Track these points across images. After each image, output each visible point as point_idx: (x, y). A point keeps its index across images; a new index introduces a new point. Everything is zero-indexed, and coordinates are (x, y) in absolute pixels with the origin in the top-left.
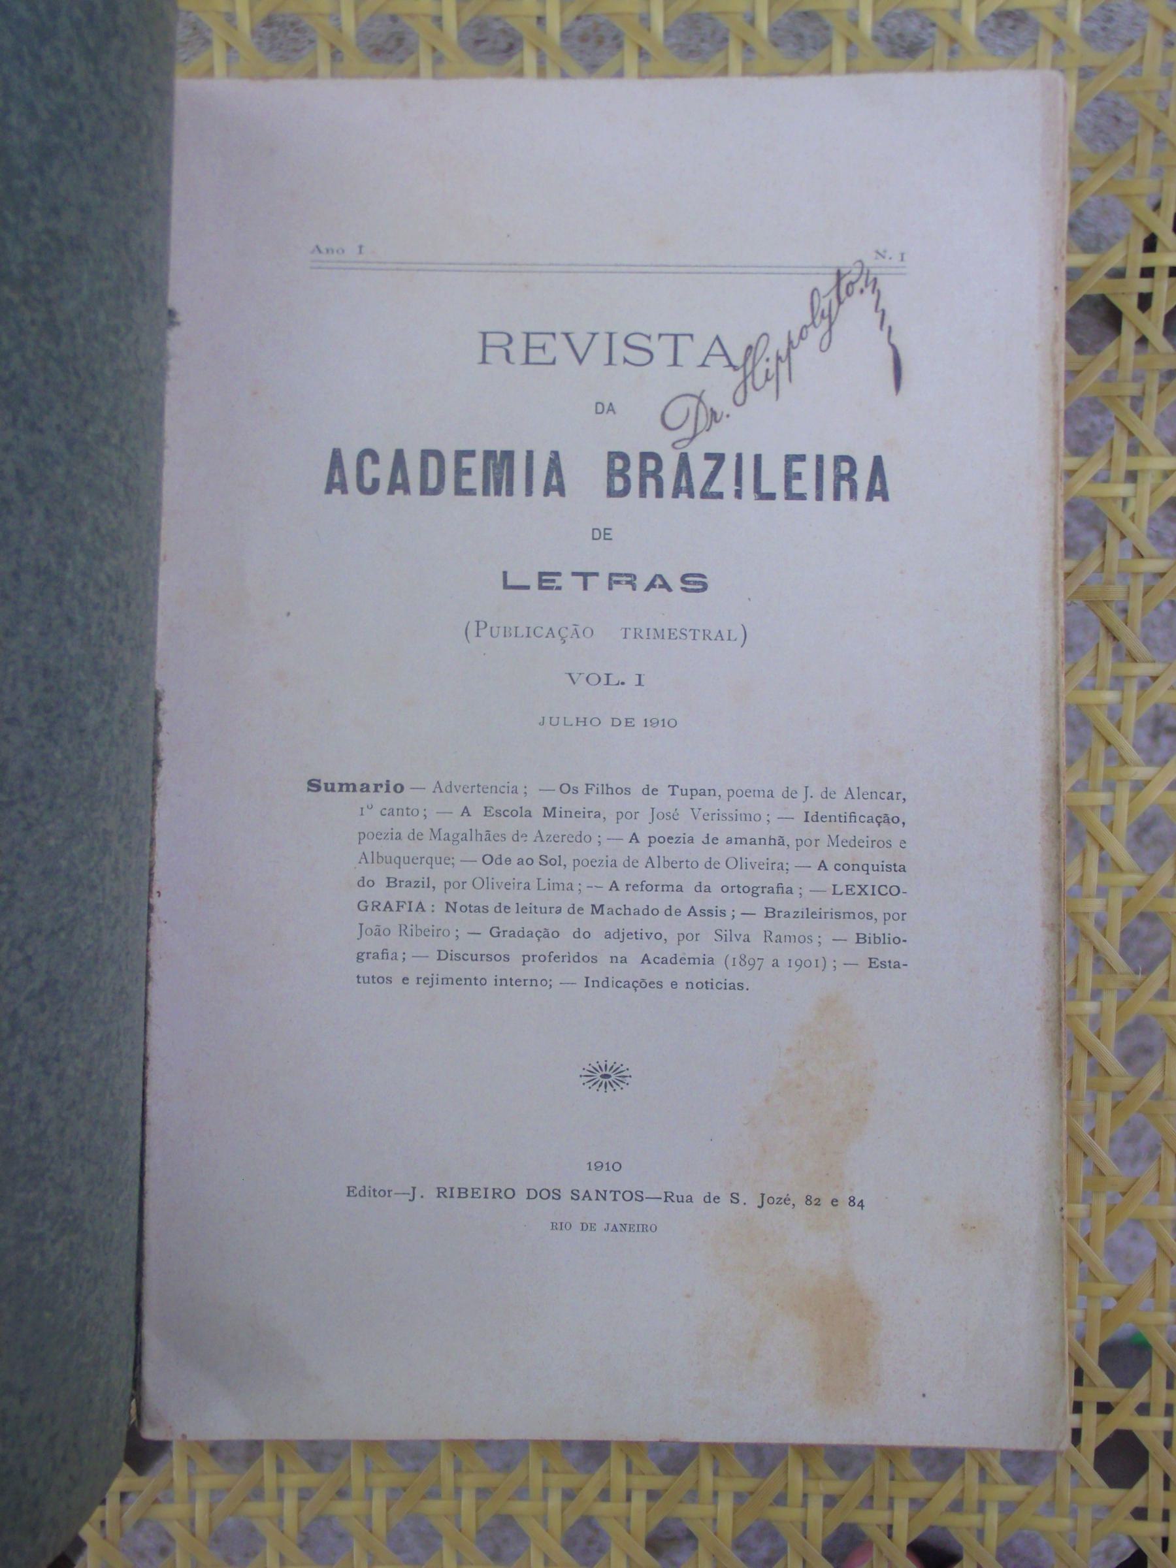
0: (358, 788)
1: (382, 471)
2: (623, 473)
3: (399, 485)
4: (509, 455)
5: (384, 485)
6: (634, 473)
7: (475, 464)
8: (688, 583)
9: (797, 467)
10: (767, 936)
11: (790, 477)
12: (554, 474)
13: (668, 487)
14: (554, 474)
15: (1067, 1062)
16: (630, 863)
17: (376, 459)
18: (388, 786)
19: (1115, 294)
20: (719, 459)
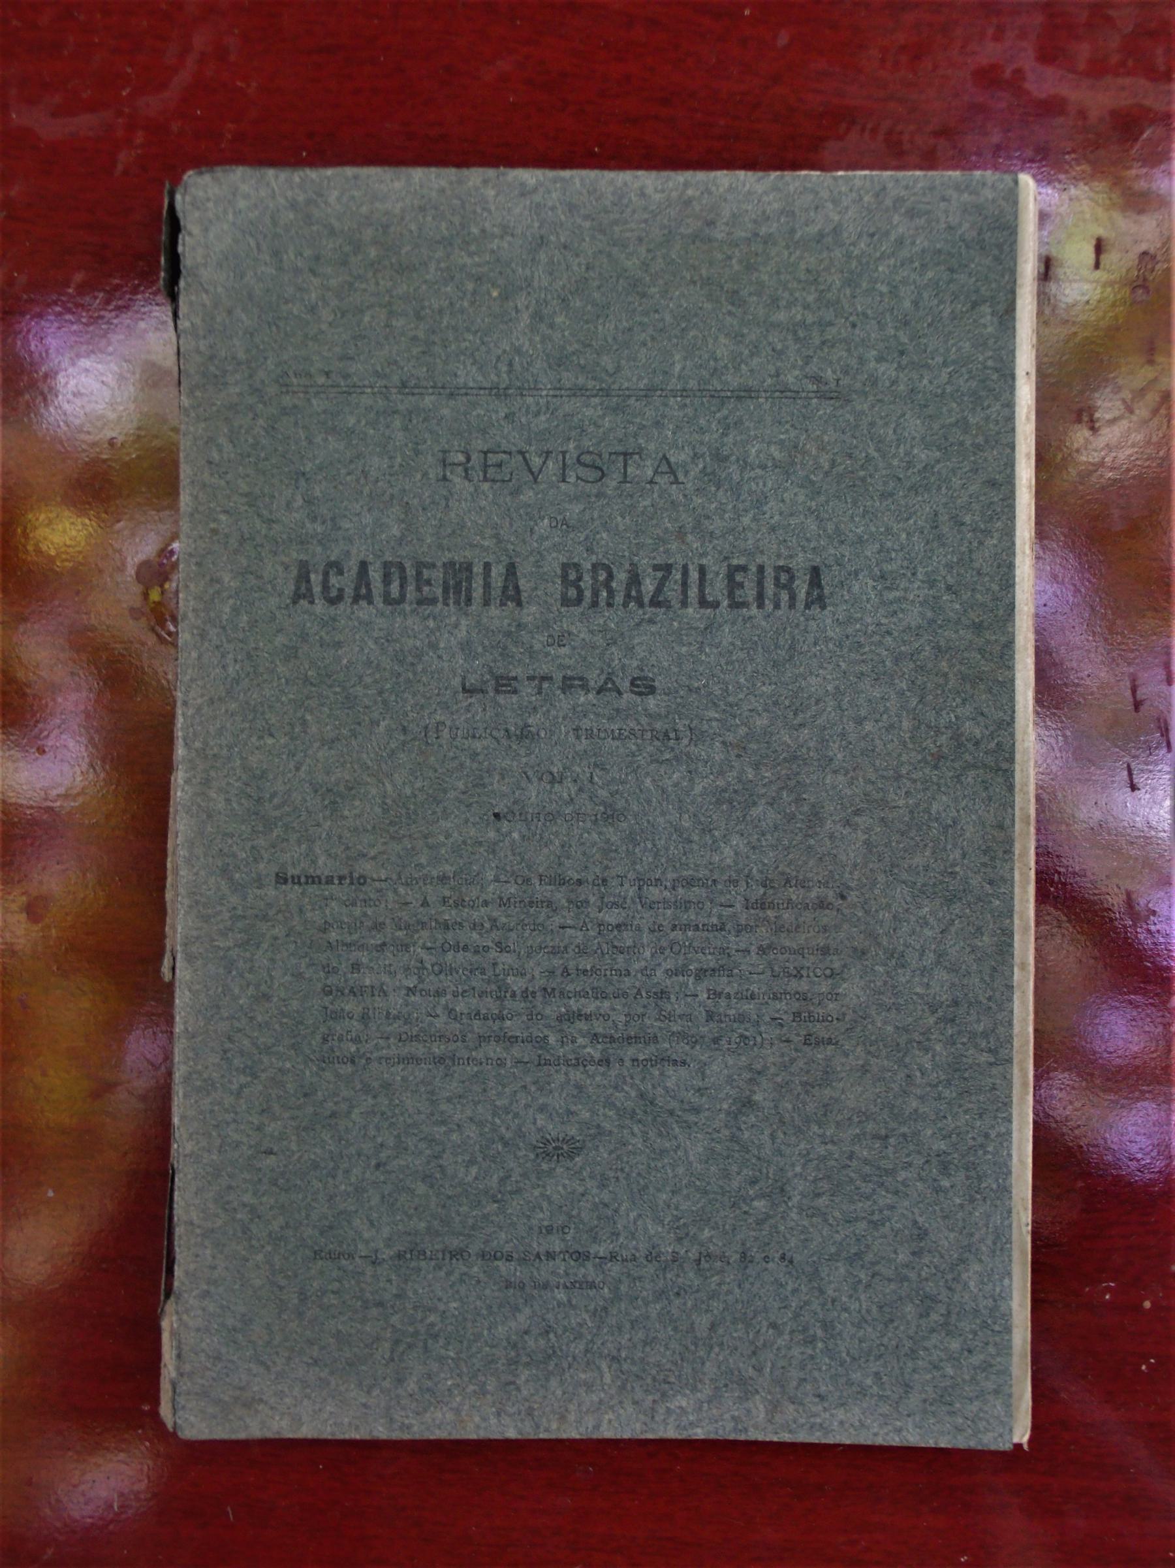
0: (323, 881)
1: (344, 582)
2: (576, 584)
3: (362, 594)
4: (469, 567)
5: (349, 592)
6: (587, 582)
7: (437, 575)
8: (638, 686)
9: (739, 578)
10: (710, 1016)
11: (733, 585)
12: (120, 167)
13: (619, 599)
14: (120, 167)
15: (474, 595)
16: (582, 951)
17: (341, 572)
18: (351, 878)
19: (762, 178)
20: (667, 568)
